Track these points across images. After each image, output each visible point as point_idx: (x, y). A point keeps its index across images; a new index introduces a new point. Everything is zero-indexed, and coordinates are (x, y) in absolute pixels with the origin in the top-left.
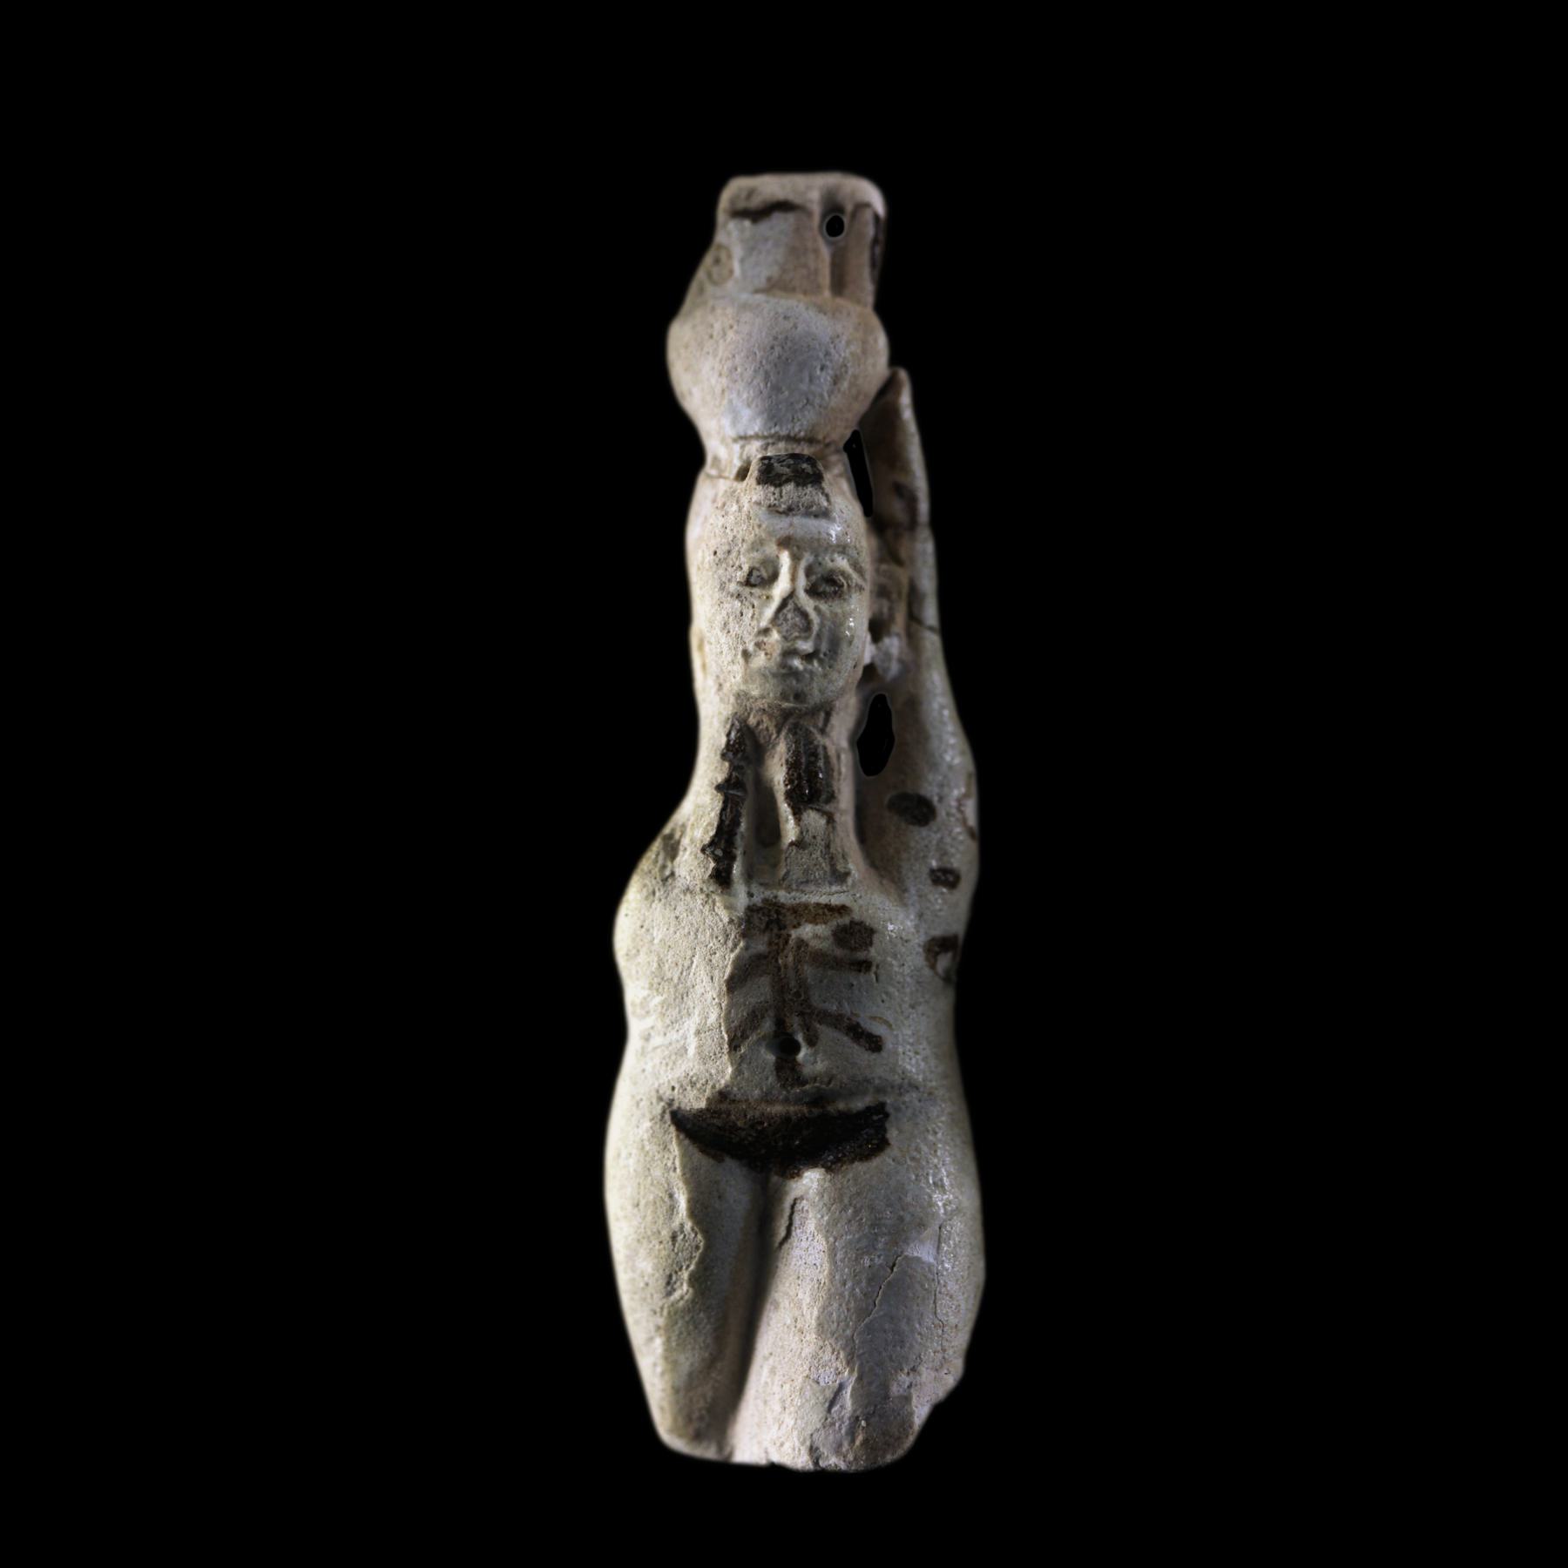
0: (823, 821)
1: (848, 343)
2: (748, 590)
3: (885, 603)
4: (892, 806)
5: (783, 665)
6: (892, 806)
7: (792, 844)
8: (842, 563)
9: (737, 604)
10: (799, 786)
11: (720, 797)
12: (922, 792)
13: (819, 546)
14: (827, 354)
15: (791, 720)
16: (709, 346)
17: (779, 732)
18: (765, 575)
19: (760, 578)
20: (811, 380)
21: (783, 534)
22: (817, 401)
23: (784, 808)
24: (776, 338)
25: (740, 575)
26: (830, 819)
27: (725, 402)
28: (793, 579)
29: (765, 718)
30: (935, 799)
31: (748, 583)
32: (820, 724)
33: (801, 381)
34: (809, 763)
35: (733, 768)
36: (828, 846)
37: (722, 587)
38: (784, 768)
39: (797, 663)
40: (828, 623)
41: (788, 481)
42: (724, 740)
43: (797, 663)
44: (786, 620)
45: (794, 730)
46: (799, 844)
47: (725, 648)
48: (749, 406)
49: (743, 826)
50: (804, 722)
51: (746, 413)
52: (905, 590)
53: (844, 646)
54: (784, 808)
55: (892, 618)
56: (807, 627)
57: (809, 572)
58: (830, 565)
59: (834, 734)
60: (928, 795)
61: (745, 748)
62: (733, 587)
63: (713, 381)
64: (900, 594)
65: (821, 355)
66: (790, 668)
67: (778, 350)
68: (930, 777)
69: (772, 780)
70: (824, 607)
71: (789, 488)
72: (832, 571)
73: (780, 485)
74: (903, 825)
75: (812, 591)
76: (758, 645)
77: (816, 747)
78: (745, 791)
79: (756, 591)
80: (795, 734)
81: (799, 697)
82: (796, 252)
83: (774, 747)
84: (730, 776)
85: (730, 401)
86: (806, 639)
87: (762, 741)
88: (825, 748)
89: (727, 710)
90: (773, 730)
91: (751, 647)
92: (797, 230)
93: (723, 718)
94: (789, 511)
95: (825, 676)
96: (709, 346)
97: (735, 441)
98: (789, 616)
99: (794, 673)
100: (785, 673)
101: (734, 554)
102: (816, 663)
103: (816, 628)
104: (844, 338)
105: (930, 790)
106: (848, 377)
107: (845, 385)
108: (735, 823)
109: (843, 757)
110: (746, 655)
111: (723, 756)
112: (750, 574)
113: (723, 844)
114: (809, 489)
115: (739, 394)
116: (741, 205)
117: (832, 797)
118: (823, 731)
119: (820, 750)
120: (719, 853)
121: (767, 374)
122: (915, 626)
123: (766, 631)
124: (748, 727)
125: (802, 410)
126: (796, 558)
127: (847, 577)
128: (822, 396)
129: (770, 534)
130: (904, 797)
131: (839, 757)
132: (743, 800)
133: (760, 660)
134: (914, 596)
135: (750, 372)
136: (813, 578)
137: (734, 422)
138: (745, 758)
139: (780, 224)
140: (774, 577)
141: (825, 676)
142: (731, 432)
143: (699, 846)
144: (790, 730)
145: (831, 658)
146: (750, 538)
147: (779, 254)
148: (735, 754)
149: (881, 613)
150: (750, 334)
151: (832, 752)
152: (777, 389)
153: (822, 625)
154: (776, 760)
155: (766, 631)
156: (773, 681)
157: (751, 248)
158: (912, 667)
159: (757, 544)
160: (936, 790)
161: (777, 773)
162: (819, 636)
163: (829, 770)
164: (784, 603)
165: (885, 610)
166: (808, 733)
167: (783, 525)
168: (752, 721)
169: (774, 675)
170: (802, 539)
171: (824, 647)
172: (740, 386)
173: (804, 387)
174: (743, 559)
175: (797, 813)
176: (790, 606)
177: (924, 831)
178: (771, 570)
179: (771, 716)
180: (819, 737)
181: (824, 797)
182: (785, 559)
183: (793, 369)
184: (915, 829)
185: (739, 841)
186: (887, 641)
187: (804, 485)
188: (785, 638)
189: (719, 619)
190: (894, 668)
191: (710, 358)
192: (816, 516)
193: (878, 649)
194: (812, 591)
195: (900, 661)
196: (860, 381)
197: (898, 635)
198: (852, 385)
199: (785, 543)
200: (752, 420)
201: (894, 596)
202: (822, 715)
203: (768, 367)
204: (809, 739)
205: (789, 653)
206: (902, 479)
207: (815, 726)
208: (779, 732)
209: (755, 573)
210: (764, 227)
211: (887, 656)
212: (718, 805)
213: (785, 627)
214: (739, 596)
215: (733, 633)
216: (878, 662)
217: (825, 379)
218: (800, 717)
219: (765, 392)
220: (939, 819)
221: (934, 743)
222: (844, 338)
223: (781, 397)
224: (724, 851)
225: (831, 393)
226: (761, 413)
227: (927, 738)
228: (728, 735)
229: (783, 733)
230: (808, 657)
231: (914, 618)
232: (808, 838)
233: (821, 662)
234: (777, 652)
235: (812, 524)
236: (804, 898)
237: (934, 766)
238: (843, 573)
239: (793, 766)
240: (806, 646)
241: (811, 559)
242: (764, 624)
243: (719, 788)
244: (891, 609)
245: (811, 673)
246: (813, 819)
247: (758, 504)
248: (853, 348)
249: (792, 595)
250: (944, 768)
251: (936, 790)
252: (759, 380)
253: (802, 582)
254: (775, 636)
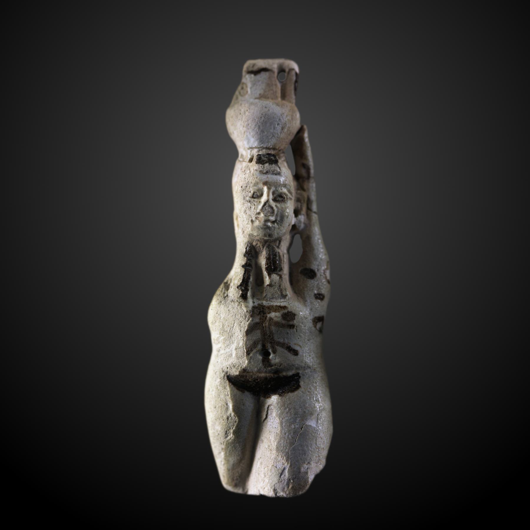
0: (278, 278)
1: (287, 116)
2: (253, 199)
3: (299, 204)
4: (302, 272)
5: (265, 225)
6: (302, 272)
7: (268, 285)
8: (285, 190)
9: (249, 204)
10: (270, 266)
11: (243, 269)
12: (312, 268)
13: (277, 185)
14: (280, 120)
15: (267, 244)
16: (240, 117)
17: (263, 248)
18: (258, 194)
19: (257, 195)
20: (274, 129)
21: (265, 180)
22: (276, 135)
23: (265, 273)
24: (262, 114)
25: (250, 194)
26: (281, 277)
27: (245, 136)
28: (268, 196)
29: (259, 243)
30: (316, 270)
31: (253, 197)
32: (277, 245)
33: (271, 129)
34: (274, 258)
35: (248, 259)
36: (280, 286)
37: (244, 198)
38: (265, 260)
39: (269, 224)
40: (280, 211)
41: (266, 163)
42: (245, 250)
43: (269, 224)
44: (266, 209)
45: (268, 247)
46: (270, 285)
47: (245, 219)
48: (253, 137)
49: (251, 279)
50: (272, 244)
51: (252, 140)
52: (306, 199)
53: (285, 218)
54: (265, 273)
55: (301, 209)
56: (273, 212)
57: (273, 193)
58: (281, 191)
59: (282, 248)
60: (314, 269)
61: (252, 253)
62: (248, 198)
63: (241, 129)
64: (304, 201)
65: (278, 120)
66: (267, 226)
67: (263, 118)
68: (314, 263)
69: (261, 264)
70: (278, 205)
71: (267, 165)
72: (281, 193)
73: (264, 164)
74: (305, 279)
75: (275, 200)
76: (256, 218)
77: (276, 253)
78: (252, 267)
79: (256, 200)
80: (269, 248)
81: (270, 235)
82: (269, 85)
83: (262, 252)
84: (247, 262)
85: (247, 136)
86: (272, 216)
87: (258, 250)
88: (279, 253)
89: (246, 240)
90: (261, 247)
91: (254, 219)
92: (269, 78)
93: (244, 243)
94: (267, 173)
95: (279, 228)
96: (240, 117)
97: (248, 149)
98: (267, 208)
99: (268, 228)
100: (265, 227)
101: (248, 187)
102: (276, 224)
103: (276, 212)
104: (285, 114)
105: (314, 267)
106: (287, 127)
107: (286, 130)
108: (249, 278)
109: (285, 256)
110: (252, 221)
111: (245, 256)
112: (254, 194)
113: (244, 285)
114: (274, 165)
115: (250, 133)
116: (251, 69)
117: (281, 269)
118: (278, 247)
119: (277, 254)
120: (243, 288)
121: (259, 126)
122: (309, 212)
123: (259, 213)
124: (253, 246)
125: (271, 138)
126: (269, 189)
127: (286, 195)
128: (278, 134)
129: (260, 180)
130: (306, 269)
131: (283, 256)
132: (251, 270)
133: (257, 223)
134: (309, 202)
135: (254, 126)
136: (275, 195)
137: (248, 143)
138: (252, 256)
139: (264, 76)
140: (262, 195)
141: (279, 228)
142: (247, 146)
143: (236, 286)
144: (267, 247)
145: (281, 222)
146: (254, 182)
147: (263, 86)
148: (248, 255)
149: (298, 207)
150: (253, 113)
151: (281, 254)
152: (262, 131)
153: (278, 211)
154: (262, 257)
155: (259, 213)
156: (261, 230)
157: (254, 84)
158: (308, 225)
159: (256, 184)
160: (316, 267)
161: (263, 261)
162: (277, 215)
163: (280, 260)
164: (265, 204)
165: (299, 206)
166: (273, 248)
167: (265, 177)
168: (254, 244)
169: (262, 228)
170: (271, 182)
171: (279, 219)
172: (250, 130)
173: (272, 131)
174: (251, 189)
175: (269, 275)
176: (267, 205)
177: (312, 281)
178: (260, 193)
179: (260, 242)
180: (277, 249)
181: (278, 269)
182: (265, 189)
183: (268, 125)
184: (309, 280)
185: (250, 284)
186: (300, 217)
187: (272, 164)
188: (265, 216)
189: (243, 209)
190: (302, 226)
191: (240, 121)
192: (276, 174)
193: (297, 219)
194: (275, 200)
195: (304, 223)
196: (291, 129)
197: (303, 215)
198: (288, 130)
199: (265, 183)
200: (254, 142)
201: (302, 201)
202: (278, 242)
203: (260, 124)
204: (273, 250)
205: (267, 221)
206: (305, 162)
207: (276, 245)
208: (263, 248)
209: (255, 194)
210: (258, 77)
211: (300, 222)
212: (243, 272)
213: (265, 212)
214: (250, 201)
215: (248, 214)
216: (297, 224)
217: (279, 128)
218: (270, 242)
219: (259, 133)
220: (317, 277)
221: (316, 251)
222: (285, 114)
223: (264, 134)
224: (245, 288)
225: (281, 133)
226: (257, 140)
227: (313, 249)
228: (246, 248)
229: (265, 248)
230: (273, 222)
231: (309, 209)
232: (273, 283)
233: (277, 224)
234: (263, 220)
235: (275, 177)
236: (272, 304)
237: (316, 259)
238: (285, 194)
239: (268, 259)
240: (273, 218)
241: (274, 189)
242: (258, 211)
243: (243, 266)
244: (301, 206)
245: (274, 227)
246: (275, 277)
247: (256, 170)
248: (288, 118)
249: (268, 201)
250: (319, 260)
251: (316, 267)
252: (256, 128)
253: (271, 197)
254: (262, 215)
